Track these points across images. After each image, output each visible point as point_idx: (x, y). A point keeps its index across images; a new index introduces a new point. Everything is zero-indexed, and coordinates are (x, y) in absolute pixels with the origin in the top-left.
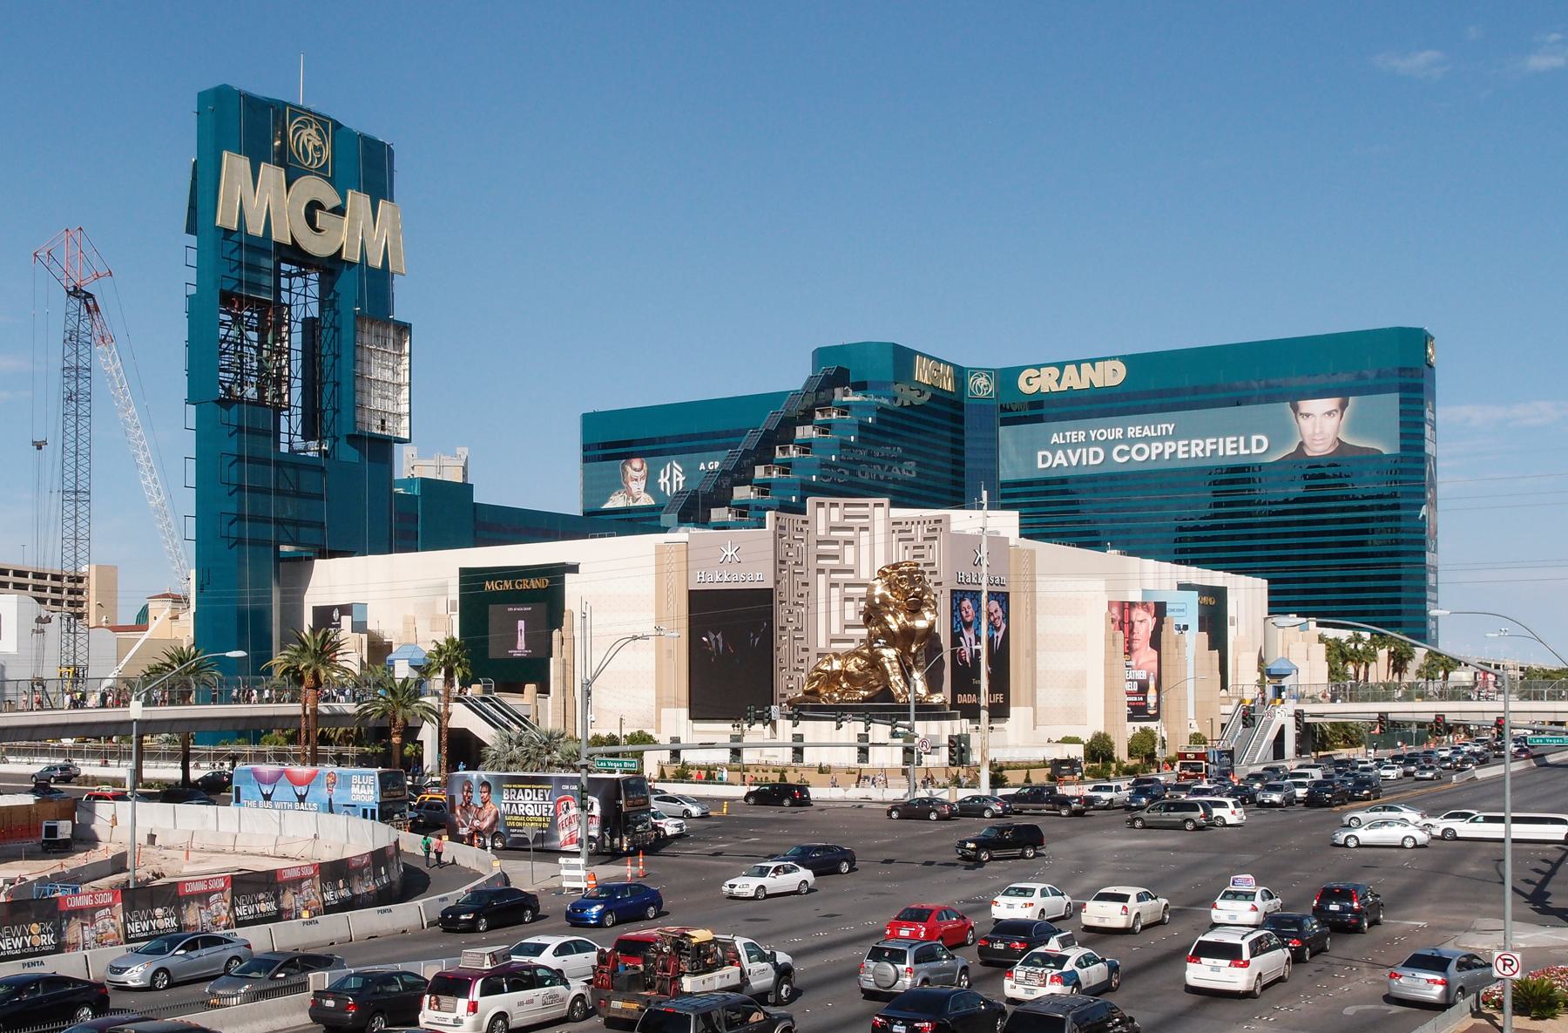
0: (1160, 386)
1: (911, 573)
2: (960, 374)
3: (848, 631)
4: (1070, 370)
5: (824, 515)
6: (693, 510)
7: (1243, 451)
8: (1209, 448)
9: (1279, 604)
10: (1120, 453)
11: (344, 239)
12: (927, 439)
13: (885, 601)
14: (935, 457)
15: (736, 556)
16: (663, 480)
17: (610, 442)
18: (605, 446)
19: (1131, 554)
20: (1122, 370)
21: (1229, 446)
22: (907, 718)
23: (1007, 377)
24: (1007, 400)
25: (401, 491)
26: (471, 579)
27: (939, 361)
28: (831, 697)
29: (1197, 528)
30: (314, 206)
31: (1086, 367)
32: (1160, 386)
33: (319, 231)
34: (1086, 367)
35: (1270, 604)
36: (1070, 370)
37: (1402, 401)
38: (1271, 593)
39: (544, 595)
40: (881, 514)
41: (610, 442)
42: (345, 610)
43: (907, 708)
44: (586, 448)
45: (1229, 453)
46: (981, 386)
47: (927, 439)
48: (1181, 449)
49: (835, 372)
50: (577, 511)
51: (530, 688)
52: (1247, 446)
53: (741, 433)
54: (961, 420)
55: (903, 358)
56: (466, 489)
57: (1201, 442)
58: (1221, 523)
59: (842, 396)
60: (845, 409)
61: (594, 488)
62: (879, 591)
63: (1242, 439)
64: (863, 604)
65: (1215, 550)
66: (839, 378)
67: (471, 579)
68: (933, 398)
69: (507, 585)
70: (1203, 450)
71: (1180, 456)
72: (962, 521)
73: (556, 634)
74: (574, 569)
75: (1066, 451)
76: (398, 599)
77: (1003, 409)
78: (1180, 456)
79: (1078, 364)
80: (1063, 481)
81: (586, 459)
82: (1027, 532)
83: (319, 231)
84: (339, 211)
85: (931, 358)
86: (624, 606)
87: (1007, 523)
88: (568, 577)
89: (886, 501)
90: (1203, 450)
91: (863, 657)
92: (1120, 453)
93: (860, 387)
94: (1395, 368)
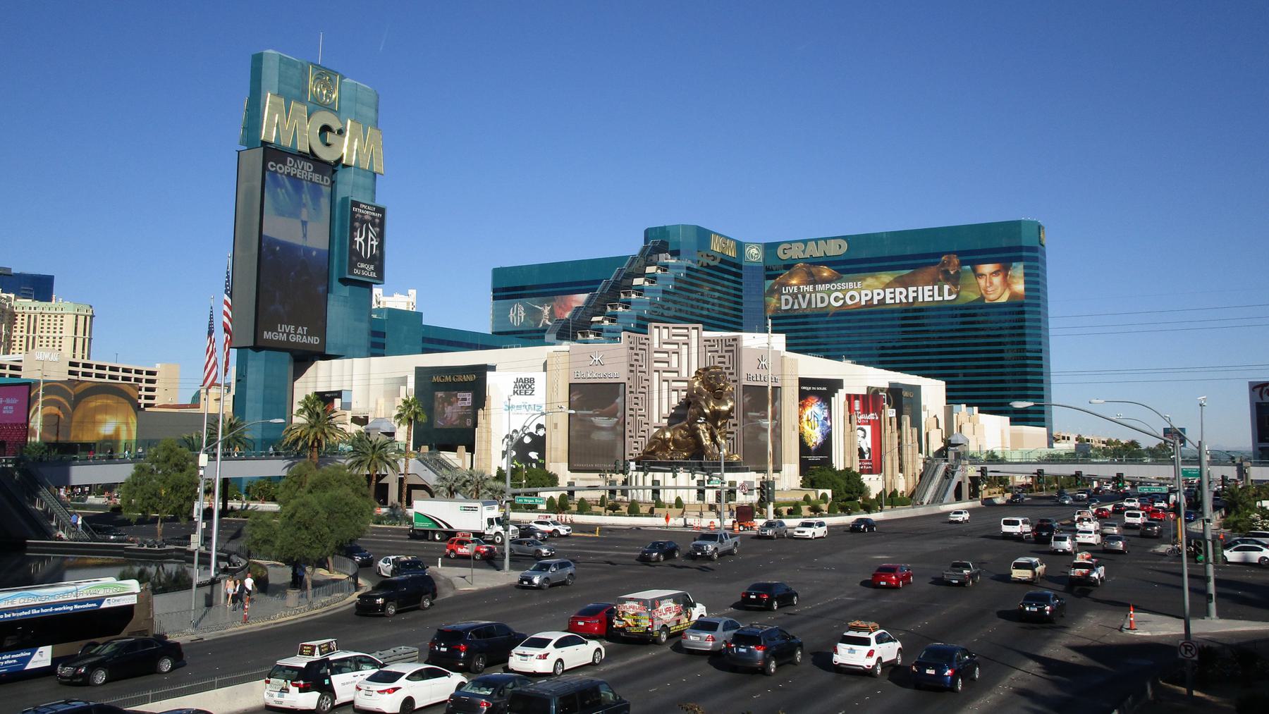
0: (860, 259)
1: (717, 374)
2: (740, 247)
3: (666, 347)
4: (812, 245)
5: (658, 334)
6: (567, 332)
7: (937, 298)
8: (911, 295)
9: (953, 397)
10: (836, 299)
11: (345, 151)
12: (721, 289)
13: (700, 393)
14: (1013, 343)
15: (604, 359)
16: (511, 315)
17: (509, 287)
18: (507, 289)
19: (859, 363)
20: (845, 245)
21: (927, 293)
22: (719, 470)
23: (770, 248)
24: (770, 263)
25: (375, 316)
26: (421, 372)
27: (727, 238)
28: (664, 457)
29: (894, 348)
30: (325, 129)
31: (821, 243)
32: (860, 259)
33: (328, 145)
34: (821, 243)
35: (947, 398)
36: (812, 245)
37: (1025, 267)
38: (947, 390)
39: (474, 383)
40: (696, 335)
41: (509, 287)
42: (339, 394)
43: (719, 464)
44: (495, 291)
45: (927, 299)
46: (754, 254)
47: (721, 289)
48: (888, 296)
49: (658, 243)
50: (488, 330)
51: (462, 449)
52: (941, 293)
53: (599, 282)
54: (739, 275)
55: (703, 235)
56: (419, 315)
57: (903, 290)
58: (899, 340)
59: (665, 258)
60: (665, 268)
61: (499, 316)
62: (696, 384)
63: (936, 287)
64: (684, 394)
65: (990, 382)
66: (662, 247)
67: (421, 372)
68: (722, 261)
69: (448, 379)
70: (907, 297)
71: (888, 301)
72: (751, 341)
73: (480, 412)
74: (493, 368)
75: (798, 294)
76: (370, 388)
77: (768, 269)
78: (888, 301)
79: (816, 240)
80: (806, 316)
81: (495, 298)
82: (790, 347)
83: (328, 145)
84: (341, 132)
85: (721, 236)
86: (524, 393)
87: (779, 340)
88: (489, 373)
89: (700, 326)
90: (907, 297)
91: (685, 430)
92: (836, 299)
93: (675, 254)
94: (1011, 246)
